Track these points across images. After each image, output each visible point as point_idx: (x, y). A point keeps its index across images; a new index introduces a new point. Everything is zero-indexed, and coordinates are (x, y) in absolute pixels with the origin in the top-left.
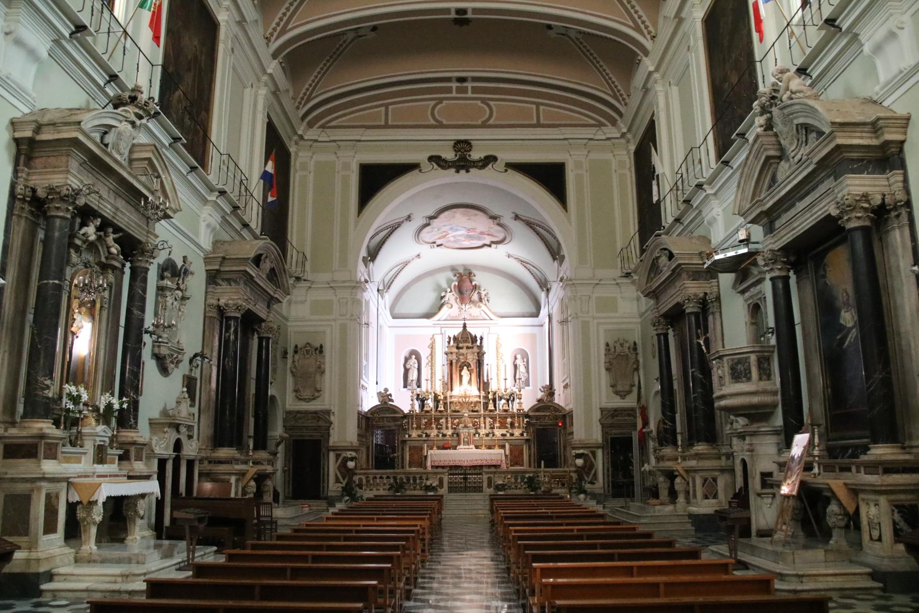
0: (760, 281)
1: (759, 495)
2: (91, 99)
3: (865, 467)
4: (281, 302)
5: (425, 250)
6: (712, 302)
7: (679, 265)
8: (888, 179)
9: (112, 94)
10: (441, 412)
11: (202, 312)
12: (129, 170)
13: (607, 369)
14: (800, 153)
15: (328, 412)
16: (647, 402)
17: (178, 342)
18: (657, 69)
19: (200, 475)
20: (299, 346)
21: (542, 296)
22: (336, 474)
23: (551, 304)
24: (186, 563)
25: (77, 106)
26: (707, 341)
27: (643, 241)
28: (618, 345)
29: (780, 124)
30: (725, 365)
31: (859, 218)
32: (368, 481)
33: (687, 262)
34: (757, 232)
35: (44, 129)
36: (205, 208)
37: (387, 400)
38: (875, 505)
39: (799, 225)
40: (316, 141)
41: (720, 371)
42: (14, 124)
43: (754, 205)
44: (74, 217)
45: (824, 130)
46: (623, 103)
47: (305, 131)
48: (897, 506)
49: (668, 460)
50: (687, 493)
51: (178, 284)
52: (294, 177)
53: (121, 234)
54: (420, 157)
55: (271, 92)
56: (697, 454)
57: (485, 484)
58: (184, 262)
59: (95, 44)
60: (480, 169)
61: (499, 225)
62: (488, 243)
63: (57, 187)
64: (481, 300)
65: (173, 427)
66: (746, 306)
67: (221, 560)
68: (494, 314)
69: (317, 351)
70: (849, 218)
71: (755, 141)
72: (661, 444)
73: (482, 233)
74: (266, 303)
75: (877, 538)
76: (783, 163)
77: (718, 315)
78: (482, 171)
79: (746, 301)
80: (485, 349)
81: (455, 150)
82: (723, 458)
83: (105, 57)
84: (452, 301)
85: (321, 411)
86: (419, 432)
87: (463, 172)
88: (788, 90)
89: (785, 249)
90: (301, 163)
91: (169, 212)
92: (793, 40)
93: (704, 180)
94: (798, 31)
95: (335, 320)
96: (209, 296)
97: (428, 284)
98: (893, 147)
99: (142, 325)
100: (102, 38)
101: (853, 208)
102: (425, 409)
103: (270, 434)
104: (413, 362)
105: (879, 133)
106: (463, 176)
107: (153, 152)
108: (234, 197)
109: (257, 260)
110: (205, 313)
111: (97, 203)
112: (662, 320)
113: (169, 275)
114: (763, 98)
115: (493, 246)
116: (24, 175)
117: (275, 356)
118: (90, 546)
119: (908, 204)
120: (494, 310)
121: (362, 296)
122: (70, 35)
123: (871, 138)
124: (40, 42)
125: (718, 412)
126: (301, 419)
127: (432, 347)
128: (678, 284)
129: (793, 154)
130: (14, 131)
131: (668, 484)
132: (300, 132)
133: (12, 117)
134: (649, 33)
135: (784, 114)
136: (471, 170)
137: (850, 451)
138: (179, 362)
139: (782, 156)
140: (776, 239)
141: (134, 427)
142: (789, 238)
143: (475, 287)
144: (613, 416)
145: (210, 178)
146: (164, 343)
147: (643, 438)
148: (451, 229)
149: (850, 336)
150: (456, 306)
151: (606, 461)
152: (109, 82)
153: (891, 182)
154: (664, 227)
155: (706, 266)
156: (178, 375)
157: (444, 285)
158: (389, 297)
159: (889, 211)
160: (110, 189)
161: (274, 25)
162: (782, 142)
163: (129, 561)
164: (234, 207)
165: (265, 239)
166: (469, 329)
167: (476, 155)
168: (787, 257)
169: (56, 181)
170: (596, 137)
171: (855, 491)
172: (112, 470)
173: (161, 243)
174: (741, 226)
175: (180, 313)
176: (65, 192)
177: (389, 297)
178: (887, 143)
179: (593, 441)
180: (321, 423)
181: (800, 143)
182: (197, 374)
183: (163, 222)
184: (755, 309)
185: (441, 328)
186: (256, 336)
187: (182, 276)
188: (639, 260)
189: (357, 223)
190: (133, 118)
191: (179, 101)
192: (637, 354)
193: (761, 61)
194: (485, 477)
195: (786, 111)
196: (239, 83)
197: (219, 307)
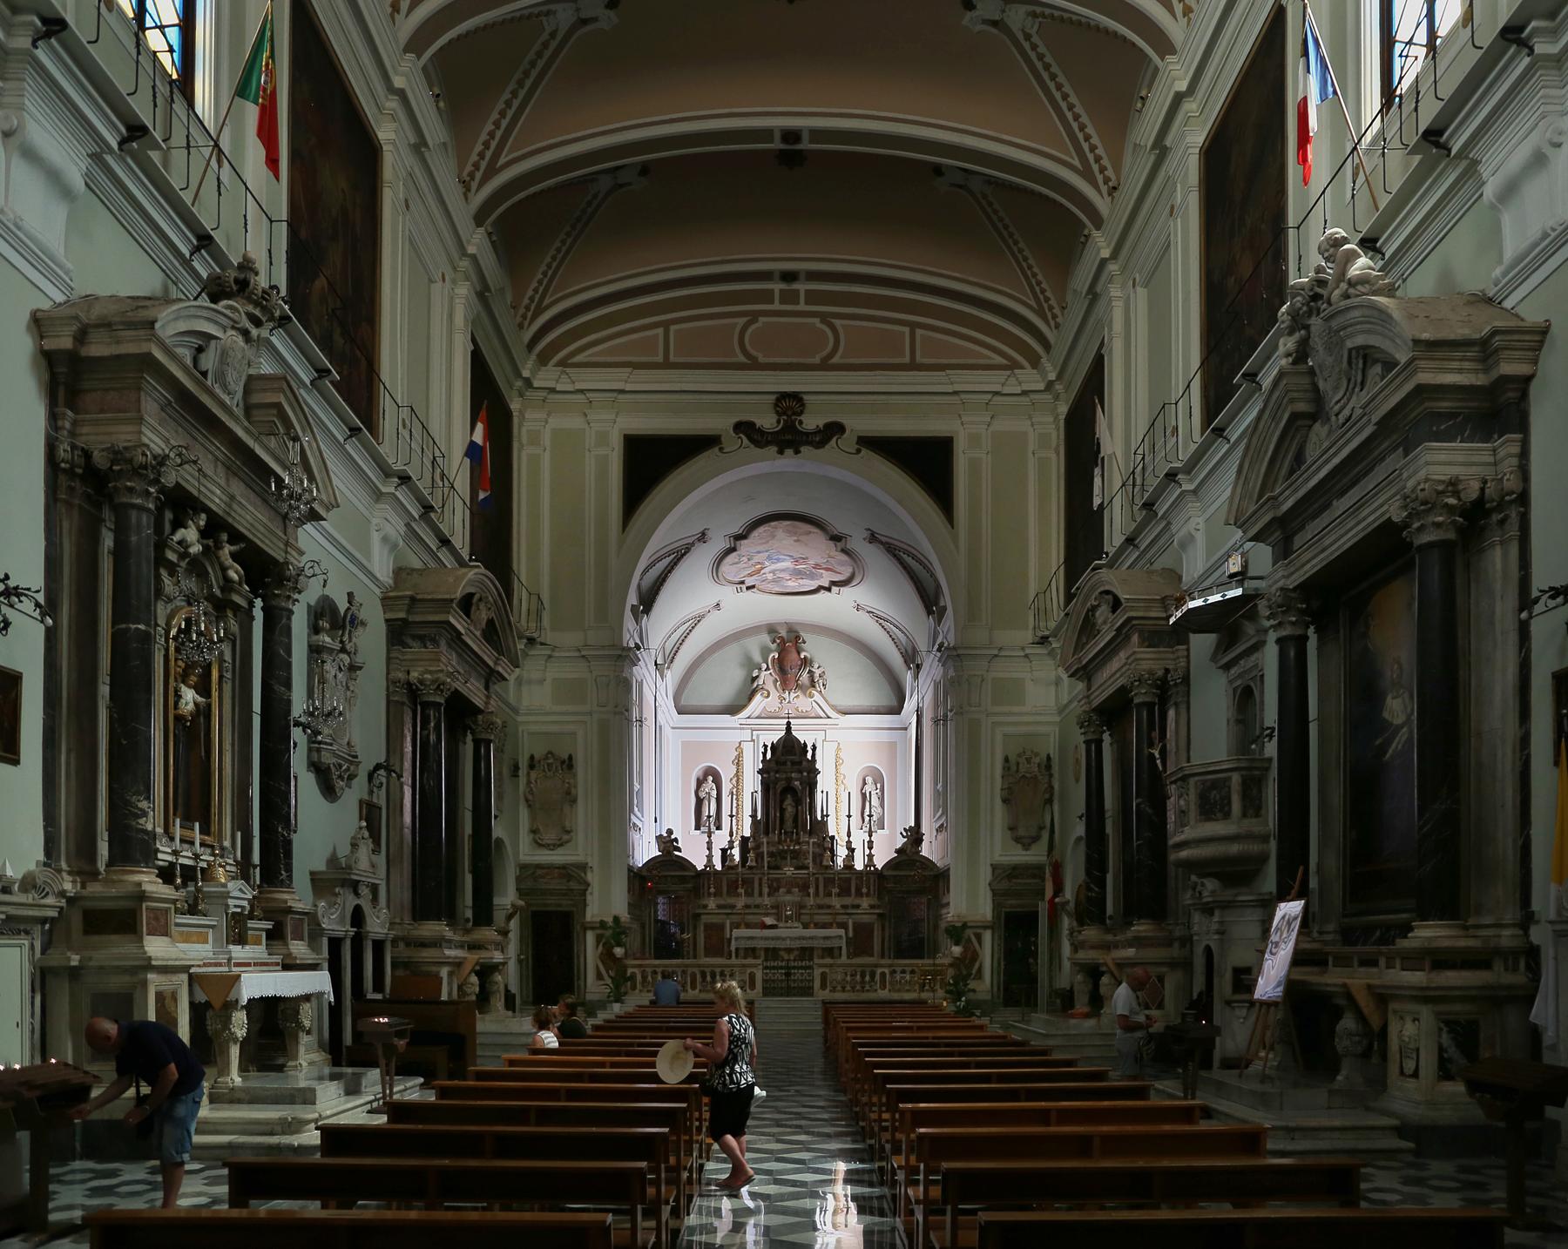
0: (1258, 646)
1: (1228, 1003)
2: (170, 282)
3: (1403, 959)
4: (504, 679)
5: (728, 596)
6: (1176, 684)
9: (205, 275)
10: (751, 868)
12: (246, 424)
13: (1005, 801)
15: (583, 867)
18: (1115, 255)
20: (537, 757)
22: (597, 967)
23: (920, 694)
24: (381, 1102)
25: (147, 294)
26: (1163, 752)
27: (1071, 577)
28: (1022, 760)
31: (1438, 525)
32: (644, 978)
33: (1141, 614)
34: (1262, 555)
36: (378, 506)
38: (1414, 1020)
40: (553, 390)
42: (39, 323)
43: (1262, 506)
44: (160, 510)
45: (1397, 356)
46: (1052, 323)
47: (534, 372)
48: (1447, 1023)
49: (1093, 947)
51: (342, 642)
52: (519, 458)
53: (243, 545)
55: (476, 293)
57: (817, 984)
58: (349, 602)
59: (165, 167)
61: (844, 551)
63: (126, 448)
64: (813, 684)
67: (431, 1097)
68: (834, 708)
70: (1422, 525)
72: (1081, 923)
74: (483, 681)
75: (1411, 1073)
76: (1317, 426)
78: (819, 452)
79: (1231, 682)
81: (777, 412)
82: (1176, 945)
83: (187, 197)
84: (770, 686)
85: (572, 865)
87: (789, 452)
89: (1305, 588)
90: (528, 431)
91: (316, 506)
93: (1179, 465)
97: (733, 652)
99: (289, 712)
101: (1430, 505)
103: (496, 901)
104: (710, 785)
106: (787, 463)
108: (423, 485)
109: (467, 604)
110: (388, 696)
112: (1094, 718)
113: (327, 625)
114: (1299, 298)
115: (834, 589)
119: (1523, 498)
120: (833, 703)
121: (632, 674)
122: (121, 144)
123: (1476, 371)
125: (1172, 870)
126: (543, 877)
127: (738, 762)
129: (1337, 408)
130: (42, 338)
131: (1090, 986)
132: (526, 374)
133: (35, 307)
134: (1107, 180)
135: (1330, 327)
136: (802, 449)
137: (1378, 933)
138: (351, 777)
139: (1317, 412)
140: (1292, 569)
141: (288, 883)
142: (1314, 566)
143: (806, 662)
144: (1010, 877)
146: (326, 743)
147: (1054, 912)
148: (769, 558)
149: (1397, 739)
150: (774, 694)
153: (1498, 457)
154: (1107, 554)
156: (353, 795)
157: (757, 658)
161: (474, 158)
162: (1321, 385)
167: (811, 422)
169: (123, 437)
170: (1007, 390)
171: (1382, 998)
172: (257, 955)
173: (309, 565)
174: (1234, 549)
175: (348, 693)
177: (672, 677)
178: (1505, 380)
179: (978, 918)
180: (573, 885)
181: (1351, 386)
182: (380, 799)
183: (308, 527)
184: (1246, 698)
186: (469, 737)
187: (348, 628)
188: (1062, 614)
192: (1051, 776)
193: (1298, 228)
194: (817, 972)
195: (1334, 324)
197: (409, 684)
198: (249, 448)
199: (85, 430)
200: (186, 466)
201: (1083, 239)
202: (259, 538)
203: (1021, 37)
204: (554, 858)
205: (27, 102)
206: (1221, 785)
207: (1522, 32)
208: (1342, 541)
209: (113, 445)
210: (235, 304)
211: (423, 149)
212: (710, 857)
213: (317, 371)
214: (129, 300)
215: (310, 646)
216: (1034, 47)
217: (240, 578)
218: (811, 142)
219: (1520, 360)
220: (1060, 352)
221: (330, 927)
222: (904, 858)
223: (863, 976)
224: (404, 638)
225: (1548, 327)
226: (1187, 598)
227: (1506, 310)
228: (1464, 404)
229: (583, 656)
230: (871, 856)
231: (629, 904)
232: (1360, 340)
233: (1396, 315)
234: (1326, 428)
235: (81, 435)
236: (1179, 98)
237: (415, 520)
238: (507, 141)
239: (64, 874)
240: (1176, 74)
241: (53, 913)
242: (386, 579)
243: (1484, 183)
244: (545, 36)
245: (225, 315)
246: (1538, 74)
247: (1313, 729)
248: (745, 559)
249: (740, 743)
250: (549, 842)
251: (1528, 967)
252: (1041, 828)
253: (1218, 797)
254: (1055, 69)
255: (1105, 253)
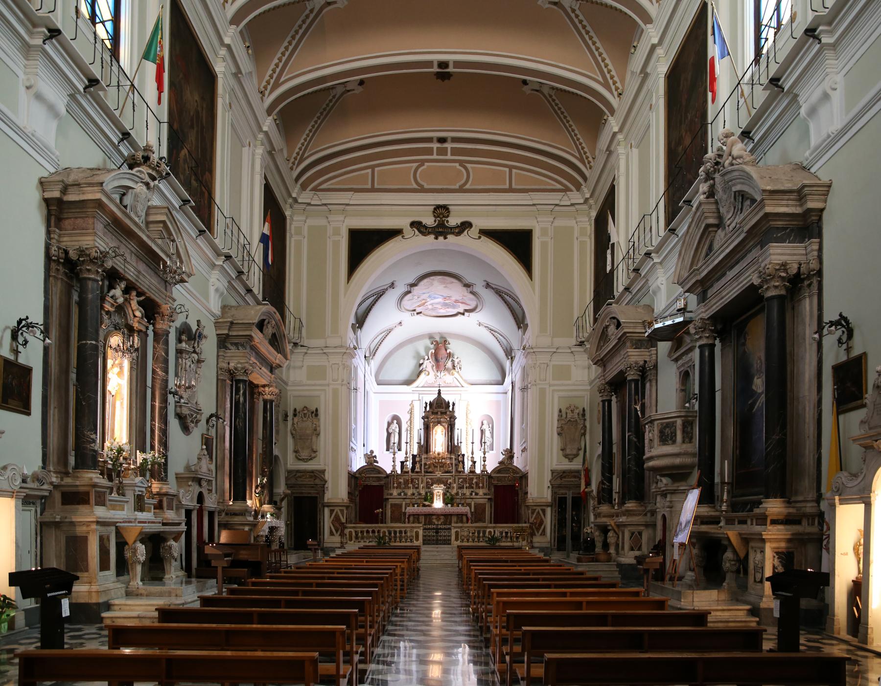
0: (691, 349)
3: (757, 519)
5: (406, 317)
7: (625, 333)
8: (806, 247)
9: (126, 154)
11: (215, 375)
13: (559, 434)
14: (735, 221)
15: (323, 472)
16: (591, 464)
17: (196, 403)
18: (621, 130)
19: (219, 525)
20: (298, 410)
21: (507, 364)
23: (514, 374)
26: (643, 407)
27: (597, 309)
28: (569, 411)
29: (720, 191)
30: (656, 429)
31: (776, 287)
34: (693, 299)
35: (71, 190)
36: (213, 272)
37: (373, 462)
39: (728, 294)
40: (309, 204)
41: (651, 434)
42: (43, 184)
46: (588, 166)
47: (298, 194)
48: (777, 553)
49: (604, 516)
50: (617, 545)
51: (194, 347)
54: (403, 222)
55: (267, 152)
56: (627, 511)
57: (453, 538)
58: (198, 326)
60: (457, 236)
61: (472, 293)
62: (462, 311)
63: (86, 249)
64: (454, 367)
65: (196, 481)
66: (678, 374)
68: (465, 381)
69: (313, 415)
71: (697, 209)
72: (599, 503)
73: (457, 301)
76: (720, 231)
77: (654, 384)
78: (459, 237)
79: (678, 368)
80: (456, 414)
81: (434, 216)
82: (649, 515)
83: (117, 113)
84: (429, 369)
85: (316, 470)
86: (399, 491)
87: (441, 238)
88: (730, 155)
89: (714, 318)
92: (742, 101)
93: (652, 248)
94: (747, 89)
95: (328, 385)
96: (220, 360)
98: (813, 215)
100: (112, 91)
101: (773, 277)
102: (405, 470)
104: (395, 426)
105: (803, 200)
107: (167, 215)
108: (238, 261)
109: (261, 325)
110: (217, 376)
111: (123, 267)
114: (709, 164)
115: (466, 314)
116: (56, 237)
117: (277, 419)
118: (137, 582)
119: (820, 273)
121: (351, 363)
122: (85, 89)
124: (59, 98)
125: (647, 473)
126: (300, 477)
127: (411, 412)
128: (622, 352)
129: (729, 222)
131: (603, 538)
132: (294, 195)
134: (617, 89)
136: (448, 236)
137: (749, 507)
138: (198, 422)
139: (720, 225)
140: (707, 308)
142: (717, 307)
143: (450, 355)
144: (561, 477)
145: (217, 241)
148: (430, 297)
150: (432, 373)
151: (553, 517)
152: (122, 140)
153: (808, 251)
155: (646, 334)
156: (197, 433)
157: (423, 353)
158: (375, 363)
159: (803, 280)
160: (132, 252)
161: (267, 78)
162: (721, 210)
163: (169, 594)
164: (238, 272)
165: (267, 304)
166: (443, 396)
168: (714, 325)
170: (562, 203)
173: (179, 306)
175: (197, 375)
176: (94, 254)
178: (810, 210)
180: (317, 481)
181: (736, 211)
182: (213, 432)
183: (178, 286)
184: (685, 376)
185: (419, 394)
188: (592, 329)
189: (346, 290)
190: (147, 179)
191: (185, 160)
192: (585, 420)
193: (711, 124)
195: (726, 178)
196: (238, 142)
197: (230, 371)
198: (150, 246)
199: (65, 239)
200: (117, 258)
201: (603, 121)
202: (153, 293)
203: (569, 10)
204: (307, 466)
205: (39, 71)
206: (671, 425)
207: (815, 31)
208: (730, 294)
209: (80, 247)
210: (142, 170)
211: (239, 76)
212: (394, 466)
213: (183, 201)
214: (89, 171)
215: (177, 350)
216: (577, 16)
217: (142, 314)
218: (454, 68)
219: (818, 201)
220: (592, 181)
221: (186, 504)
222: (504, 466)
223: (479, 533)
224: (226, 344)
225: (831, 183)
226: (654, 322)
227: (812, 173)
228: (788, 223)
229: (325, 353)
230: (484, 466)
231: (348, 493)
232: (738, 188)
233: (755, 176)
234: (724, 232)
235: (63, 242)
236: (653, 47)
237: (233, 279)
238: (285, 69)
239: (52, 473)
240: (652, 34)
241: (46, 494)
242: (217, 312)
243: (801, 107)
244: (307, 12)
245: (138, 177)
246: (824, 53)
247: (718, 396)
248: (416, 297)
249: (412, 401)
250: (304, 457)
251: (819, 523)
252: (579, 449)
253: (669, 432)
254: (588, 28)
255: (616, 129)
